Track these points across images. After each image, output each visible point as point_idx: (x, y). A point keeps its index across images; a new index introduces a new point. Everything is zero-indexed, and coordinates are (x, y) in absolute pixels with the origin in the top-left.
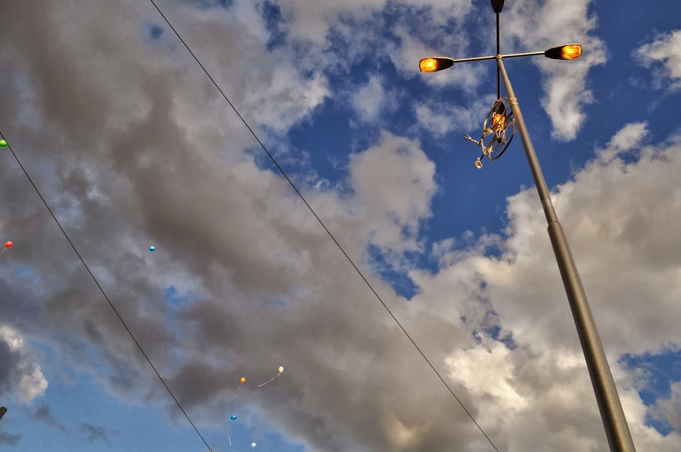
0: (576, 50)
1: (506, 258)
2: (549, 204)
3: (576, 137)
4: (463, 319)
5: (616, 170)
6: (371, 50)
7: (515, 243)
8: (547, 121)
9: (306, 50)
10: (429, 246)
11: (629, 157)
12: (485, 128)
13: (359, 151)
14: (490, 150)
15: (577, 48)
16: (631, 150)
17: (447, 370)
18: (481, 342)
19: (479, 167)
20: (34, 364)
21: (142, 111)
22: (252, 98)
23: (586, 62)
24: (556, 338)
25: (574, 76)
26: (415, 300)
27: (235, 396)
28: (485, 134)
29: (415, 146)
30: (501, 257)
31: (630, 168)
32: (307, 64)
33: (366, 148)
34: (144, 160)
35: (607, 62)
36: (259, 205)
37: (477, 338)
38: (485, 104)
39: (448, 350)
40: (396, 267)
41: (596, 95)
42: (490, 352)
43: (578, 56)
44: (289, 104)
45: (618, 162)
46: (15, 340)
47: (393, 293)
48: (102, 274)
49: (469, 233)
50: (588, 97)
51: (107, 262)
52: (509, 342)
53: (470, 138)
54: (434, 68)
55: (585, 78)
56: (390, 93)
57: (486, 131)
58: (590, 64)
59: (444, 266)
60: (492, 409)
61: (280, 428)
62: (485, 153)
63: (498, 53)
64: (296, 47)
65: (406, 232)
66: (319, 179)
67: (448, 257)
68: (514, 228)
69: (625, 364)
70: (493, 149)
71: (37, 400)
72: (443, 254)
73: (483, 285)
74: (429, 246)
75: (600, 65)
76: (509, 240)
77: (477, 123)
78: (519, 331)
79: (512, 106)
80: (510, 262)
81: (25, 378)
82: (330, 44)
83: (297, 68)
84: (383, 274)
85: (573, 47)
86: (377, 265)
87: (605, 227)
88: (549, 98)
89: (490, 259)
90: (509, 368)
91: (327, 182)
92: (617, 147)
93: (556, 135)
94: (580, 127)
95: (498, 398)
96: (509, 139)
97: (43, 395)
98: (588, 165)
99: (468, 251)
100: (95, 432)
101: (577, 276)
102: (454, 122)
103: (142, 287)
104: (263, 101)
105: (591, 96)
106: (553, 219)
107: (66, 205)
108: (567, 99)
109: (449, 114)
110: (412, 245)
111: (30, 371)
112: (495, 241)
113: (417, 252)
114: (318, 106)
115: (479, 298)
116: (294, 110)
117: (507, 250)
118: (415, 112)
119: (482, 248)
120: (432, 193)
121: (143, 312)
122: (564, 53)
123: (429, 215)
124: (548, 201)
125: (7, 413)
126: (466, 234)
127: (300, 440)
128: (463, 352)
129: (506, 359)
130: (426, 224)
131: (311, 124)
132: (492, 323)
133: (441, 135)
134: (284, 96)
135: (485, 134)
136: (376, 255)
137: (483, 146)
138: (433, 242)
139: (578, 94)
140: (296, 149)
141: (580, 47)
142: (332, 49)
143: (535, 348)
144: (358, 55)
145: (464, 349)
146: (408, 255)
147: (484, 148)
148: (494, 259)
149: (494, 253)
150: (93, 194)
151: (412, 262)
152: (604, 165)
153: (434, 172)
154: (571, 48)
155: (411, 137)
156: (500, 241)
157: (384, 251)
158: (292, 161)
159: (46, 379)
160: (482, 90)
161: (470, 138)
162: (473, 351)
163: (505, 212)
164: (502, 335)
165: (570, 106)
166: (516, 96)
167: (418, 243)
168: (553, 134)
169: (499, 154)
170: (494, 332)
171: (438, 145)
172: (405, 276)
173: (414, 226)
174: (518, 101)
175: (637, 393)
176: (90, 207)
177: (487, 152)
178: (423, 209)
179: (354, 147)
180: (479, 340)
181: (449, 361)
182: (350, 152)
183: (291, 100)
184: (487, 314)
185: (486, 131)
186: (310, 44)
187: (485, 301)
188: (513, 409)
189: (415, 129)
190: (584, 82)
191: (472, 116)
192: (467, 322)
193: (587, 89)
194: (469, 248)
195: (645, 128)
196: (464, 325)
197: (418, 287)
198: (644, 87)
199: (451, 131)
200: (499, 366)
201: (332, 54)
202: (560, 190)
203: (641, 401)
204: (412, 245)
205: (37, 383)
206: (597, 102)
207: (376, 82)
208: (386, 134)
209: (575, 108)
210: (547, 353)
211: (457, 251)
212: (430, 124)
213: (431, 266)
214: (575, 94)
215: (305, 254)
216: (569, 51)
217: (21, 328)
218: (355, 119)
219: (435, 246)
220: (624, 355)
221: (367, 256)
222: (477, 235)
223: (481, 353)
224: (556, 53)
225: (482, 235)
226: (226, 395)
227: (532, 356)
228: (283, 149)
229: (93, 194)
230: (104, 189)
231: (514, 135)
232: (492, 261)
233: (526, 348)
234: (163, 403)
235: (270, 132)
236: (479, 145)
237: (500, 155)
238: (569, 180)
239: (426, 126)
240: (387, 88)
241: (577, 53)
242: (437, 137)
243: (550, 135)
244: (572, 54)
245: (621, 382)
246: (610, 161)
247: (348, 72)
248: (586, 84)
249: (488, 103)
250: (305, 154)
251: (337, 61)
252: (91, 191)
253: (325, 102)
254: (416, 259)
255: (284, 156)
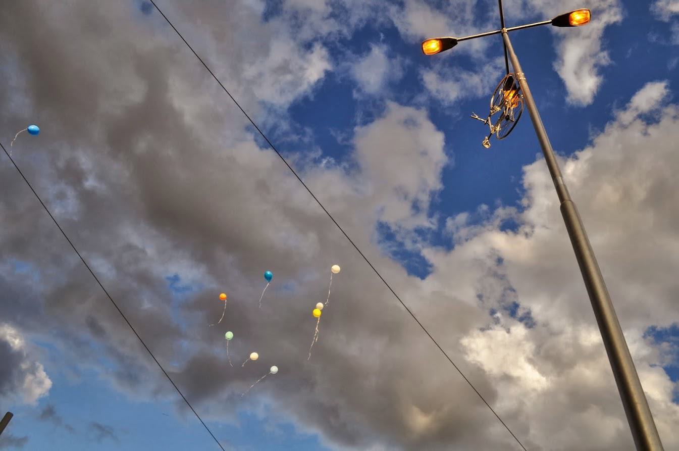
0: (584, 15)
1: (522, 232)
2: (561, 182)
3: (593, 101)
4: (480, 297)
5: (635, 133)
6: (373, 14)
7: (531, 215)
8: (560, 85)
9: (306, 18)
10: (442, 222)
11: (650, 119)
12: (492, 106)
13: (365, 123)
14: (498, 129)
15: (586, 13)
16: (651, 112)
17: (464, 351)
18: (499, 323)
19: (487, 146)
20: (37, 364)
21: (136, 93)
22: (250, 71)
23: (601, 20)
24: (575, 317)
25: (589, 37)
26: (429, 280)
27: (243, 366)
28: (492, 111)
29: (421, 116)
30: (518, 230)
31: (652, 130)
32: (306, 34)
33: (372, 121)
34: (142, 145)
35: (623, 20)
36: (262, 187)
37: (494, 318)
38: (496, 68)
39: (464, 330)
40: (409, 246)
41: (612, 56)
42: (508, 331)
43: (587, 22)
44: (289, 77)
45: (639, 125)
46: (15, 339)
47: (404, 273)
48: (102, 267)
49: (484, 207)
50: (604, 58)
51: (107, 254)
52: (528, 320)
53: (477, 117)
54: (437, 49)
55: (601, 38)
56: (394, 61)
57: (493, 109)
58: (605, 23)
59: (460, 243)
60: (513, 391)
61: (292, 417)
62: (493, 132)
63: (503, 27)
64: (295, 16)
65: (416, 207)
66: (323, 157)
67: (463, 232)
68: (530, 198)
69: (650, 338)
70: (501, 127)
71: (41, 400)
72: (457, 228)
73: (500, 261)
74: (442, 222)
75: (615, 23)
76: (526, 212)
77: (487, 88)
78: (537, 308)
79: (519, 81)
80: (527, 235)
81: (29, 378)
82: (330, 10)
83: (294, 39)
84: (395, 254)
85: (582, 12)
86: (389, 244)
87: (627, 194)
88: (563, 61)
89: (506, 233)
90: (529, 347)
91: (332, 160)
92: (637, 109)
93: (571, 100)
94: (597, 91)
95: (519, 378)
96: (517, 116)
97: (47, 394)
98: (607, 128)
99: (483, 226)
100: (103, 431)
101: (592, 255)
102: (464, 88)
103: (145, 279)
104: (260, 75)
105: (607, 57)
106: (566, 197)
107: (61, 196)
108: (582, 61)
109: (457, 80)
110: (424, 222)
111: (33, 370)
112: (511, 214)
113: (429, 229)
114: (319, 81)
115: (495, 275)
116: (295, 84)
117: (523, 223)
118: (422, 80)
119: (497, 222)
120: (442, 165)
121: (147, 304)
122: (572, 20)
123: (439, 186)
124: (559, 179)
125: (13, 418)
126: (480, 208)
127: (314, 430)
128: (480, 333)
129: (527, 339)
130: (436, 196)
131: (312, 98)
132: (510, 299)
133: (450, 102)
134: (284, 68)
135: (492, 111)
136: (387, 233)
137: (490, 124)
138: (446, 218)
139: (594, 55)
140: (298, 125)
141: (588, 12)
142: (332, 15)
143: (555, 325)
144: (361, 20)
145: (482, 330)
146: (420, 232)
147: (491, 126)
148: (510, 233)
149: (510, 226)
150: (90, 183)
151: (424, 240)
152: (624, 127)
153: (443, 143)
154: (579, 14)
155: (418, 106)
156: (516, 213)
157: (394, 228)
158: (295, 138)
159: (50, 378)
160: (491, 53)
161: (477, 117)
162: (490, 332)
163: (521, 182)
164: (520, 313)
165: (586, 69)
166: (523, 71)
167: (430, 219)
168: (568, 99)
169: (508, 132)
170: (512, 310)
171: (447, 113)
172: (418, 255)
173: (425, 199)
174: (525, 76)
175: (663, 369)
176: (87, 197)
177: (495, 131)
178: (434, 183)
179: (359, 120)
180: (497, 321)
181: (465, 341)
182: (355, 125)
183: (290, 72)
184: (505, 289)
185: (493, 109)
186: (309, 11)
187: (502, 277)
188: (534, 390)
189: (421, 98)
190: (599, 43)
191: (482, 80)
192: (484, 299)
193: (602, 50)
194: (485, 222)
195: (666, 87)
196: (481, 302)
197: (431, 266)
198: (663, 43)
199: (460, 97)
200: (519, 344)
201: (332, 21)
202: (578, 156)
203: (668, 378)
204: (424, 222)
205: (41, 383)
206: (614, 62)
207: (378, 53)
208: (392, 106)
209: (590, 71)
210: (569, 330)
211: (473, 226)
212: (438, 91)
213: (445, 242)
214: (590, 56)
215: (312, 236)
216: (577, 17)
217: (22, 325)
218: (359, 90)
219: (450, 223)
220: (649, 328)
221: (376, 236)
222: (493, 208)
223: (499, 334)
224: (564, 20)
225: (498, 208)
226: (235, 387)
227: (554, 334)
228: (285, 126)
229: (90, 183)
230: (101, 178)
231: (523, 111)
232: (508, 235)
233: (546, 325)
234: (172, 398)
235: (270, 109)
236: (487, 123)
237: (507, 135)
238: (588, 146)
239: (434, 93)
240: (390, 56)
241: (586, 19)
242: (446, 104)
243: (564, 100)
244: (581, 19)
245: (643, 359)
246: (631, 123)
247: (349, 38)
248: (602, 45)
249: (499, 66)
250: (309, 131)
251: (337, 28)
252: (87, 180)
253: (326, 75)
254: (429, 236)
255: (286, 134)
